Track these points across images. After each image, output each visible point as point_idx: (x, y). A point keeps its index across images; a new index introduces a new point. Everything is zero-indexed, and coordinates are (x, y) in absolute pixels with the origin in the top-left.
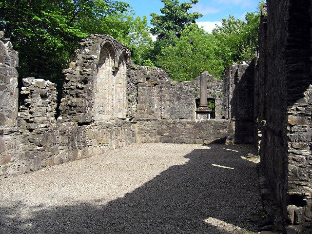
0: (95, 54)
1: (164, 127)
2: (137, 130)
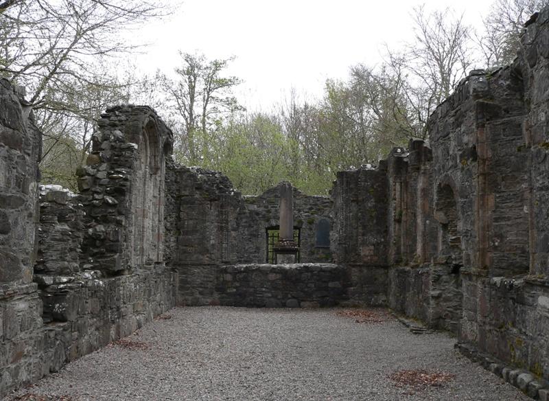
1: (229, 277)
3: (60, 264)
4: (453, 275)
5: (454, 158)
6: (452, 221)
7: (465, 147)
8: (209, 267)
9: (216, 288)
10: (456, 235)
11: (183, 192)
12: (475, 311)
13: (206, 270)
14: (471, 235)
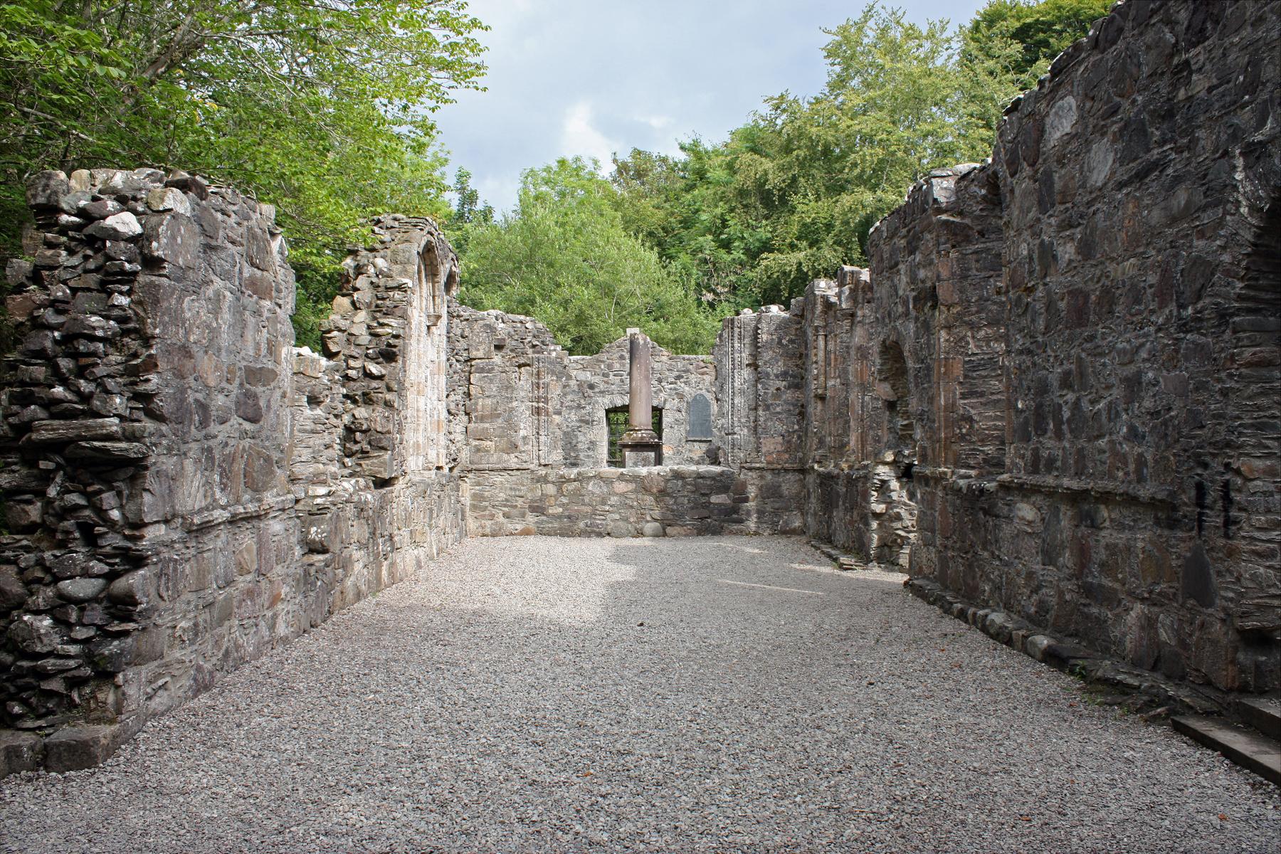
0: (404, 272)
1: (551, 489)
2: (467, 500)
3: (311, 469)
4: (905, 480)
5: (906, 303)
6: (902, 397)
7: (920, 285)
8: (518, 473)
9: (530, 507)
10: (908, 418)
11: (474, 354)
12: (933, 531)
13: (514, 478)
14: (928, 418)
